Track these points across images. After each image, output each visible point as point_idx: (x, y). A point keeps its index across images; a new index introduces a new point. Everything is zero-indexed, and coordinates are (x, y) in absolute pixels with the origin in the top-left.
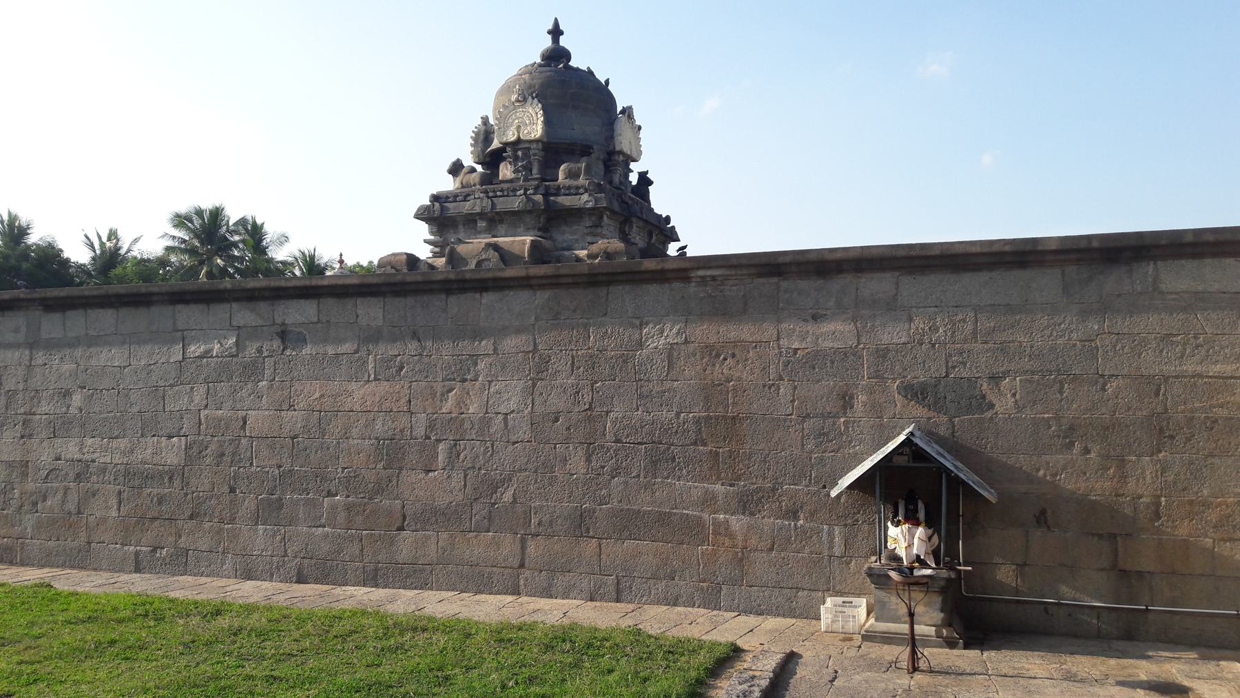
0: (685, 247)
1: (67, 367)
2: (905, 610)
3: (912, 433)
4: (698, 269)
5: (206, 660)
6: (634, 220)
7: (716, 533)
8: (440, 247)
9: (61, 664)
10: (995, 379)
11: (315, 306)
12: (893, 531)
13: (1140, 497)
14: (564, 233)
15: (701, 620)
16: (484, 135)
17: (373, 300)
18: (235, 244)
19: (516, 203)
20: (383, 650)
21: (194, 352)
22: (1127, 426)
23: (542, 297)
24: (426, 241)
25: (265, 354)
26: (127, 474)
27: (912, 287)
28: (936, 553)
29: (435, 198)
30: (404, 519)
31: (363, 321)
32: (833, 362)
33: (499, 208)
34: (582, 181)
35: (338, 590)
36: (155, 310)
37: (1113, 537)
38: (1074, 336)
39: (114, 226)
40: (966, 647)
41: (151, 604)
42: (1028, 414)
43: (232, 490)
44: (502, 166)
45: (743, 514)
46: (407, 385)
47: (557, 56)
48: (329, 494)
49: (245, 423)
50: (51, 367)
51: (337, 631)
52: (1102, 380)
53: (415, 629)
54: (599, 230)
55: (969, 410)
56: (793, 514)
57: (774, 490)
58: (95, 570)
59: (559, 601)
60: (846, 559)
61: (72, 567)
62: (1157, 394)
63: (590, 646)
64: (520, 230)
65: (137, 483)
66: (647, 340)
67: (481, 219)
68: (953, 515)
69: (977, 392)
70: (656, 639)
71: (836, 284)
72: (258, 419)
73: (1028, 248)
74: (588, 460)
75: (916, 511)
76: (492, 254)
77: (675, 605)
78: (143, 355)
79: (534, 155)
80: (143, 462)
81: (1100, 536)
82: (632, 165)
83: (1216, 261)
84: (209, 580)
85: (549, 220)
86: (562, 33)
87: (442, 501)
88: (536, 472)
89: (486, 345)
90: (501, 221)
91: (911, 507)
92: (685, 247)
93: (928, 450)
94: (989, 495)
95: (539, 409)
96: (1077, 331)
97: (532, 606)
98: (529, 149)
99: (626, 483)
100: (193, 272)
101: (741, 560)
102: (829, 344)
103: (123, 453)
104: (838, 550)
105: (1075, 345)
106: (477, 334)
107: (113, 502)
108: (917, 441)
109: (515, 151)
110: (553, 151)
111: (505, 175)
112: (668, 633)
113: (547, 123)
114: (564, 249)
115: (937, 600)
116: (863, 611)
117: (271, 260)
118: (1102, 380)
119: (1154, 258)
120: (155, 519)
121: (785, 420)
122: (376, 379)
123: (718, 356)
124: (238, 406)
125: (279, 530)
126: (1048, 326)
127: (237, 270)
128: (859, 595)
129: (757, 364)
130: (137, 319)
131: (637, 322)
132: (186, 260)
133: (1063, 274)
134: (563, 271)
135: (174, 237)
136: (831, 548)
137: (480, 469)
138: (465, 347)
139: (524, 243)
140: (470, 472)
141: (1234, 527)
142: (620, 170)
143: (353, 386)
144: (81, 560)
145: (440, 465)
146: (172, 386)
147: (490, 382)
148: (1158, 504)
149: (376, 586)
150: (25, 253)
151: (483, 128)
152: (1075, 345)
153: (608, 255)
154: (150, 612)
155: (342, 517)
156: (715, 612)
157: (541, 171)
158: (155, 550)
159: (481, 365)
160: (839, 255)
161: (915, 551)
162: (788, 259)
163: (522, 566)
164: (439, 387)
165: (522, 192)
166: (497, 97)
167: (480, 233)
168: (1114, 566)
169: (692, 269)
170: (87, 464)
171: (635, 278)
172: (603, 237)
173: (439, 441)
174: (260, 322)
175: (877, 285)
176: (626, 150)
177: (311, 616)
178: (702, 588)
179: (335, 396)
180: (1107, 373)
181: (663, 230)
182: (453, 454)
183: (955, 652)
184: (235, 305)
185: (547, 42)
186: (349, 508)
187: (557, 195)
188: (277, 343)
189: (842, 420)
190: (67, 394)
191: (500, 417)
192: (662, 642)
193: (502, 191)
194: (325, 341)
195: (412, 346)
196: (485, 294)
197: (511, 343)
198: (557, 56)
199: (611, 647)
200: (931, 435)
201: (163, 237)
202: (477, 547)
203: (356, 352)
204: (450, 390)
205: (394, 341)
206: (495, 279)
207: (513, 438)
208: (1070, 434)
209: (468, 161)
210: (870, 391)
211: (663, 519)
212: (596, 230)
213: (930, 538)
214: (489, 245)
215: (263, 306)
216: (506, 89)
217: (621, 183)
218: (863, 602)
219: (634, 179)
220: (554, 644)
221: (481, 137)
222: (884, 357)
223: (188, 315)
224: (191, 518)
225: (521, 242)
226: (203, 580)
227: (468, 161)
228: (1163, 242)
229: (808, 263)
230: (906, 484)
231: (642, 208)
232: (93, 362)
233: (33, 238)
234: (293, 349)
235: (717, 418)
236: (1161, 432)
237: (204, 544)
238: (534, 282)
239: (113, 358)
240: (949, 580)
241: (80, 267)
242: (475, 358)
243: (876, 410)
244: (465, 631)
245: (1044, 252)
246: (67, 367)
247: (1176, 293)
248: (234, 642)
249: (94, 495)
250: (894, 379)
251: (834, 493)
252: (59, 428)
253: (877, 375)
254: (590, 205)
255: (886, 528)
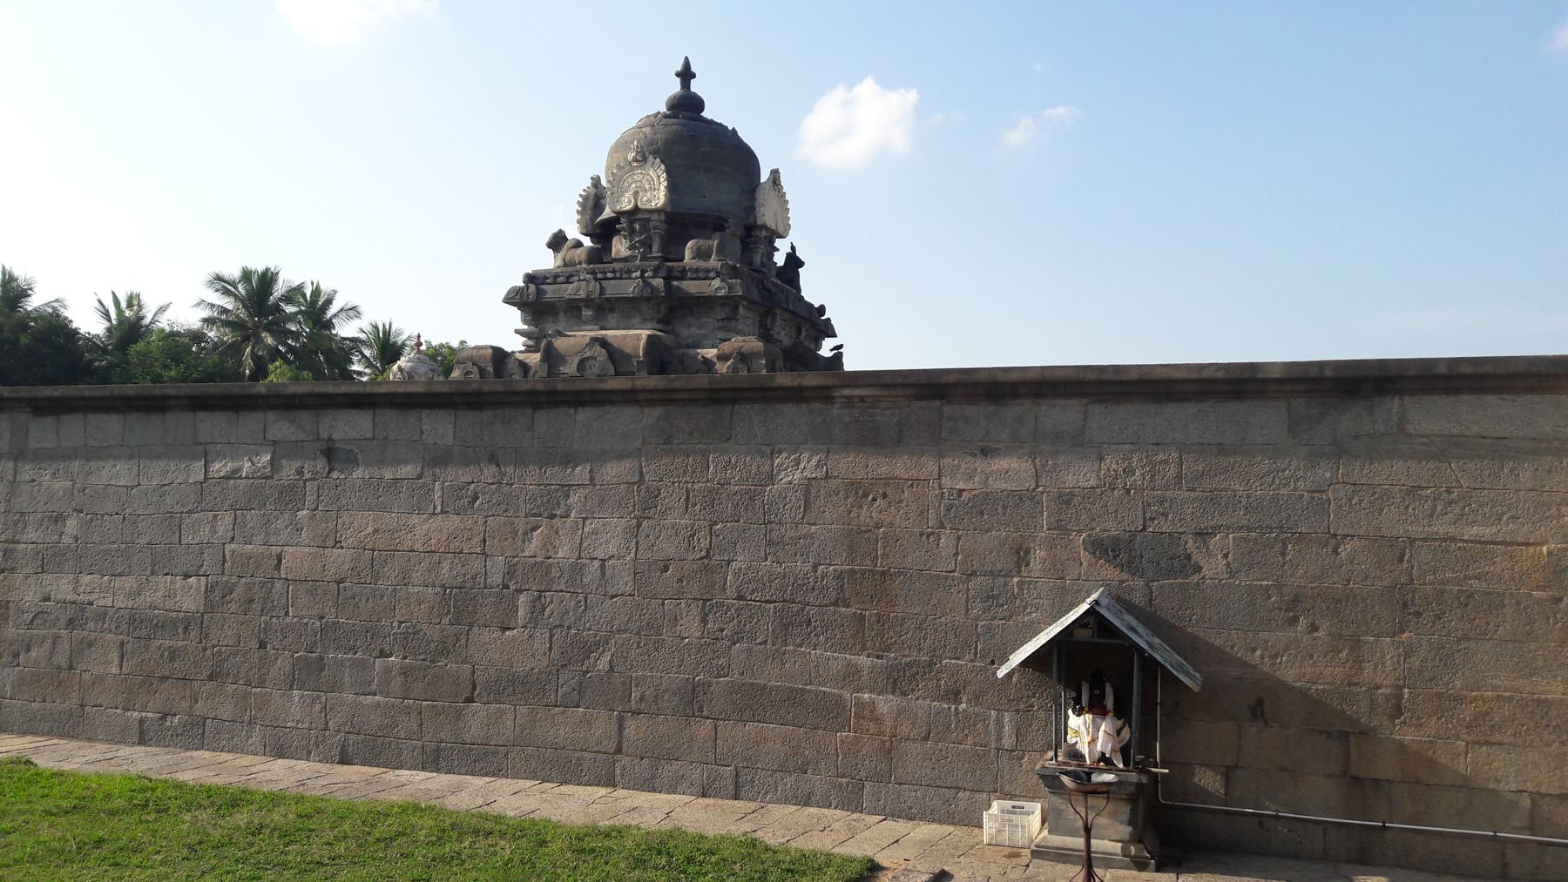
0: (841, 346)
1: (61, 484)
2: (1080, 824)
3: (1097, 602)
4: (843, 387)
5: (213, 869)
6: (778, 311)
7: (859, 716)
8: (535, 339)
9: (34, 869)
10: (1202, 535)
11: (370, 419)
12: (1074, 721)
13: (1378, 687)
14: (690, 326)
15: (836, 826)
16: (594, 201)
17: (442, 413)
18: (292, 318)
19: (630, 288)
20: (434, 859)
21: (220, 470)
22: (1364, 599)
23: (652, 415)
24: (517, 332)
25: (307, 476)
26: (132, 620)
27: (1104, 418)
28: (1125, 752)
29: (531, 278)
30: (474, 688)
31: (429, 439)
32: (1005, 508)
33: (609, 293)
34: (714, 262)
35: (391, 775)
36: (172, 418)
37: (1345, 736)
38: (1301, 485)
39: (136, 290)
40: (1159, 869)
41: (153, 790)
42: (1242, 580)
43: (262, 645)
44: (615, 240)
45: (893, 693)
46: (481, 520)
47: (687, 105)
48: (382, 654)
49: (280, 561)
50: (40, 485)
51: (380, 832)
52: (1334, 540)
53: (476, 832)
54: (733, 324)
55: (1171, 572)
56: (955, 696)
57: (931, 664)
58: (89, 740)
59: (663, 796)
60: (1017, 753)
61: (61, 736)
62: (1401, 560)
63: (690, 860)
64: (635, 321)
65: (144, 633)
66: (779, 473)
67: (587, 306)
68: (1148, 705)
69: (1180, 551)
70: (775, 852)
71: (1014, 410)
72: (297, 557)
73: (1247, 374)
74: (704, 621)
75: (1103, 696)
76: (598, 351)
77: (806, 804)
78: (157, 473)
79: (655, 228)
80: (152, 607)
81: (1329, 734)
82: (778, 243)
83: (1473, 398)
84: (230, 756)
85: (671, 310)
86: (694, 76)
87: (522, 667)
88: (639, 633)
89: (581, 472)
90: (612, 310)
91: (1097, 692)
92: (841, 346)
93: (1117, 623)
94: (1191, 680)
95: (644, 555)
96: (1305, 479)
97: (628, 804)
98: (648, 220)
99: (749, 650)
100: (235, 349)
101: (889, 751)
102: (1000, 485)
103: (129, 595)
104: (1008, 742)
105: (1301, 497)
106: (570, 460)
107: (114, 655)
108: (1103, 612)
109: (632, 222)
110: (678, 223)
111: (618, 251)
112: (793, 844)
113: (672, 188)
114: (689, 346)
115: (1125, 809)
116: (1035, 820)
117: (332, 338)
118: (1334, 540)
119: (1401, 392)
120: (164, 678)
121: (946, 578)
122: (443, 512)
123: (866, 495)
124: (272, 540)
125: (319, 697)
126: (1269, 472)
127: (291, 349)
128: (1032, 799)
129: (913, 507)
130: (147, 427)
131: (768, 450)
132: (229, 337)
133: (1289, 408)
134: (677, 385)
135: (213, 305)
136: (999, 739)
137: (569, 628)
138: (554, 475)
139: (638, 337)
140: (557, 632)
141: (1493, 727)
142: (762, 248)
143: (415, 519)
144: (72, 727)
145: (521, 622)
146: (190, 512)
147: (584, 519)
148: (1399, 696)
149: (438, 770)
150: (22, 326)
151: (593, 191)
152: (1301, 497)
153: (744, 358)
154: (150, 800)
155: (397, 682)
156: (856, 816)
157: (663, 248)
158: (164, 717)
159: (574, 499)
160: (1014, 377)
161: (1099, 748)
162: (952, 379)
163: (619, 751)
164: (521, 524)
165: (638, 274)
166: (611, 155)
167: (585, 323)
168: (1345, 773)
169: (836, 387)
170: (82, 607)
171: (764, 395)
172: (739, 333)
173: (519, 591)
174: (302, 436)
175: (1062, 414)
176: (770, 223)
177: (351, 809)
178: (841, 785)
179: (392, 532)
180: (1340, 532)
181: (816, 323)
182: (537, 608)
183: (1145, 875)
184: (271, 415)
185: (675, 87)
186: (405, 672)
187: (682, 278)
188: (321, 465)
189: (1016, 580)
190: (59, 519)
191: (597, 564)
192: (781, 857)
193: (614, 271)
194: (382, 462)
195: (490, 472)
196: (580, 410)
197: (612, 471)
198: (687, 105)
199: (717, 863)
200: (1123, 603)
201: (198, 304)
202: (563, 726)
203: (420, 477)
204: (535, 529)
205: (467, 465)
206: (593, 392)
207: (611, 591)
208: (1294, 606)
209: (573, 232)
210: (1051, 547)
211: (795, 698)
212: (729, 323)
213: (1119, 732)
214: (595, 340)
215: (305, 417)
216: (621, 146)
217: (763, 265)
218: (1037, 807)
219: (779, 259)
220: (647, 857)
221: (591, 203)
222: (1067, 503)
223: (210, 424)
224: (211, 678)
225: (634, 337)
226: (224, 756)
227: (573, 232)
228: (1411, 373)
229: (978, 384)
230: (1090, 665)
231: (787, 297)
232: (93, 480)
233: (33, 303)
234: (342, 471)
235: (863, 573)
236: (1404, 606)
237: (225, 712)
238: (641, 397)
239: (118, 476)
240: (1139, 785)
241: (91, 342)
242: (566, 489)
243: (1057, 569)
244: (534, 834)
245: (1265, 381)
246: (61, 484)
247: (1426, 436)
248: (251, 844)
249: (90, 646)
250: (1080, 531)
251: (1001, 673)
252: (47, 562)
253: (1060, 527)
254: (722, 293)
255: (1067, 717)
